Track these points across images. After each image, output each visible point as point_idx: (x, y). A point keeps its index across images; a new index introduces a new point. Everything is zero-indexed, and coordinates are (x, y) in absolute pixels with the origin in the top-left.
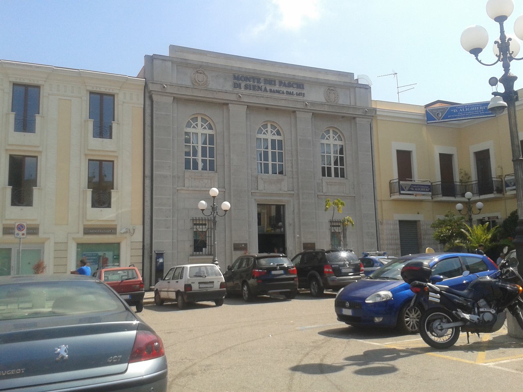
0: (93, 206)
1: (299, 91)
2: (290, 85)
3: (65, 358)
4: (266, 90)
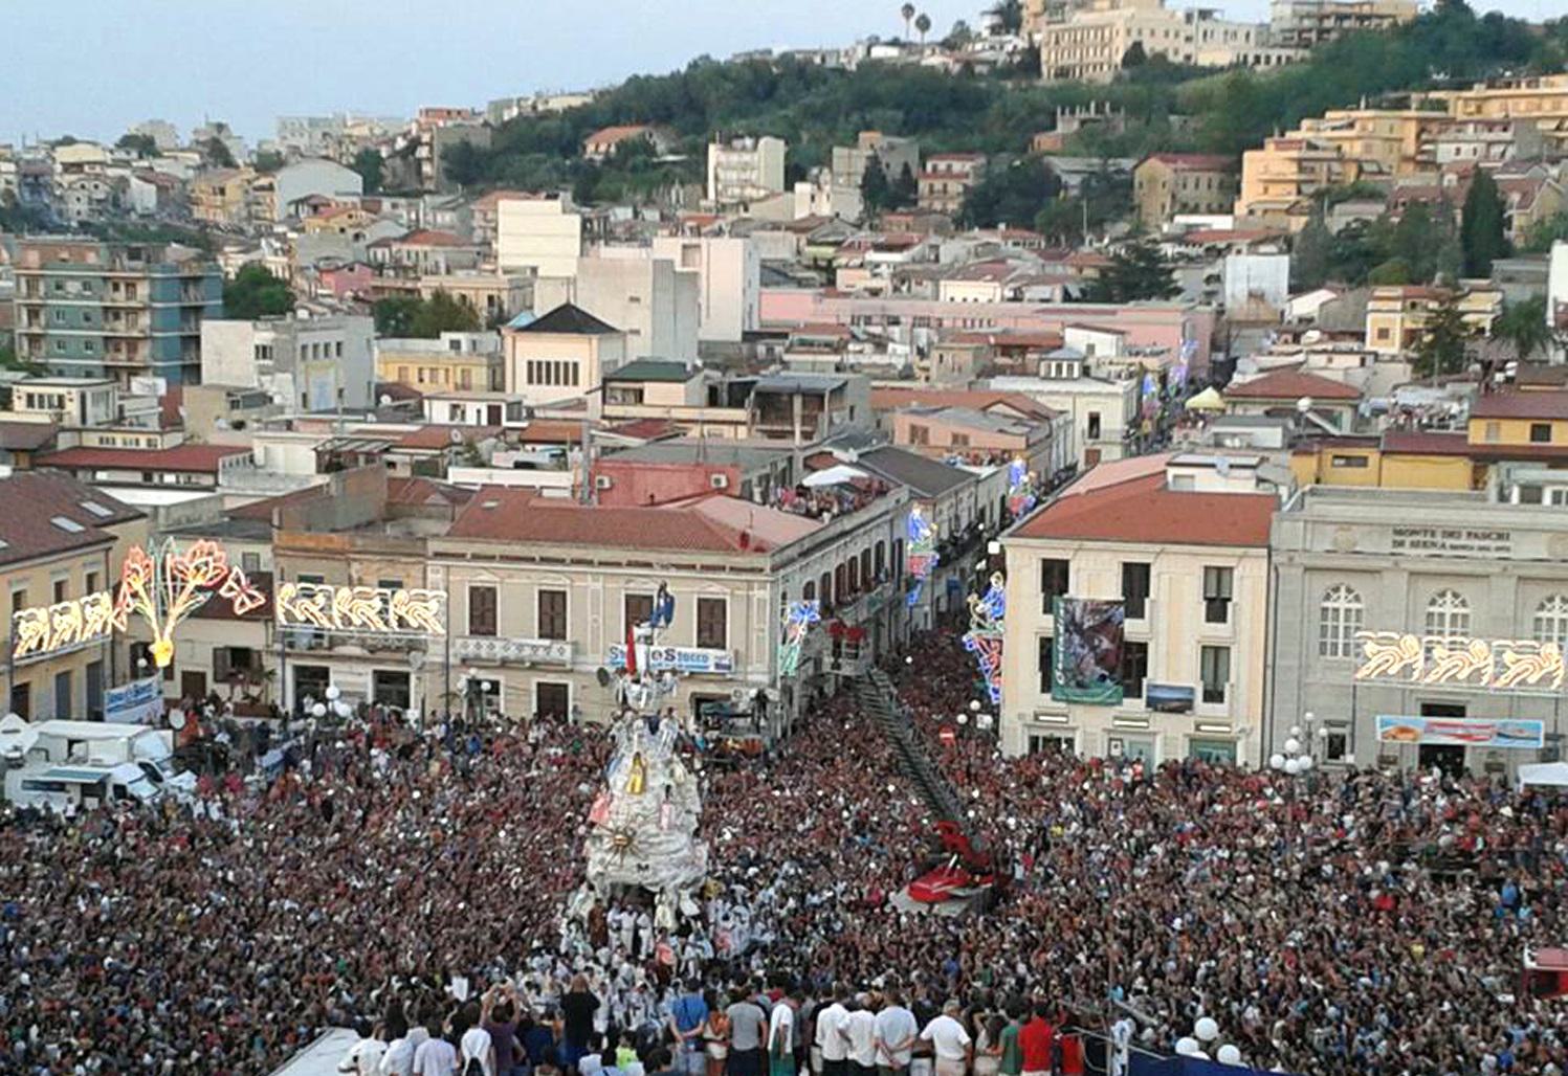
0: (1045, 561)
1: (1500, 544)
2: (1487, 536)
3: (999, 64)
4: (1443, 546)
